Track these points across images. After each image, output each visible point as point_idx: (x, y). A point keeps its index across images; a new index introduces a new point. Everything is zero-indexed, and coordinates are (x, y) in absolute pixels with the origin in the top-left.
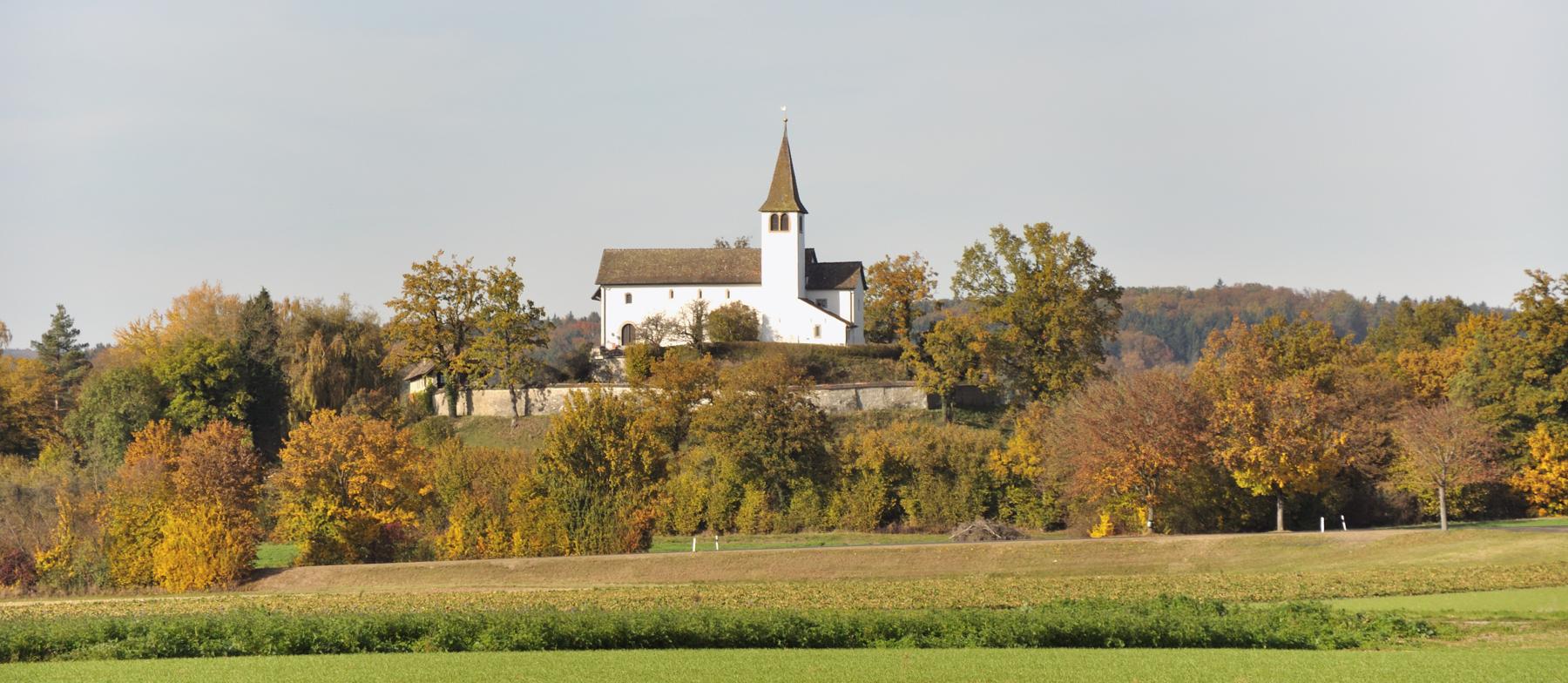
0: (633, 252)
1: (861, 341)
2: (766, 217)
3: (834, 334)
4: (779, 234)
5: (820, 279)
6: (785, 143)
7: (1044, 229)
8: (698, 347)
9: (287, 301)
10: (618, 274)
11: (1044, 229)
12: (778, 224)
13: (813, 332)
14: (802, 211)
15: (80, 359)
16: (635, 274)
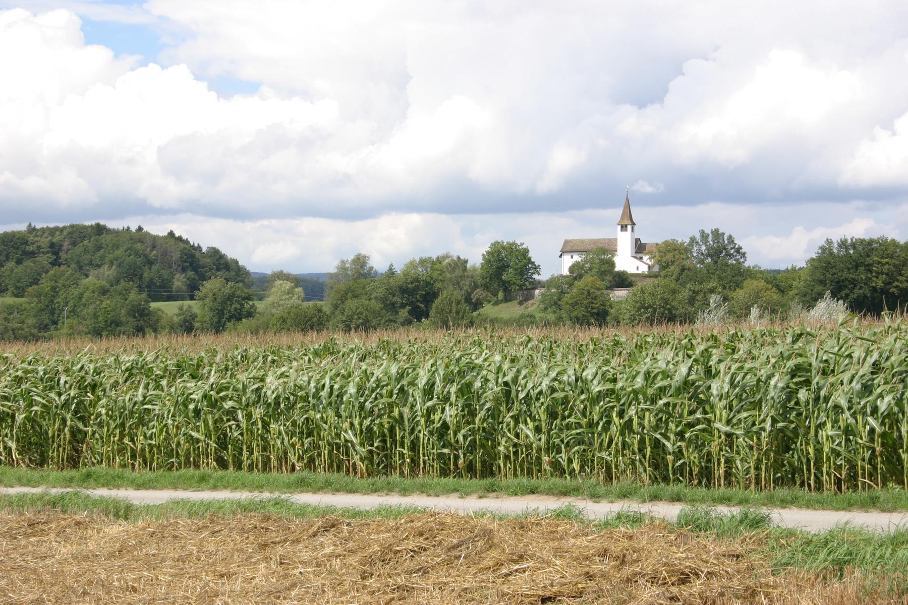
2: (619, 227)
3: (644, 269)
4: (624, 233)
5: (640, 248)
6: (627, 200)
7: (717, 230)
8: (679, 523)
9: (741, 248)
10: (568, 248)
11: (717, 230)
12: (624, 228)
14: (633, 224)
15: (393, 273)
16: (574, 248)
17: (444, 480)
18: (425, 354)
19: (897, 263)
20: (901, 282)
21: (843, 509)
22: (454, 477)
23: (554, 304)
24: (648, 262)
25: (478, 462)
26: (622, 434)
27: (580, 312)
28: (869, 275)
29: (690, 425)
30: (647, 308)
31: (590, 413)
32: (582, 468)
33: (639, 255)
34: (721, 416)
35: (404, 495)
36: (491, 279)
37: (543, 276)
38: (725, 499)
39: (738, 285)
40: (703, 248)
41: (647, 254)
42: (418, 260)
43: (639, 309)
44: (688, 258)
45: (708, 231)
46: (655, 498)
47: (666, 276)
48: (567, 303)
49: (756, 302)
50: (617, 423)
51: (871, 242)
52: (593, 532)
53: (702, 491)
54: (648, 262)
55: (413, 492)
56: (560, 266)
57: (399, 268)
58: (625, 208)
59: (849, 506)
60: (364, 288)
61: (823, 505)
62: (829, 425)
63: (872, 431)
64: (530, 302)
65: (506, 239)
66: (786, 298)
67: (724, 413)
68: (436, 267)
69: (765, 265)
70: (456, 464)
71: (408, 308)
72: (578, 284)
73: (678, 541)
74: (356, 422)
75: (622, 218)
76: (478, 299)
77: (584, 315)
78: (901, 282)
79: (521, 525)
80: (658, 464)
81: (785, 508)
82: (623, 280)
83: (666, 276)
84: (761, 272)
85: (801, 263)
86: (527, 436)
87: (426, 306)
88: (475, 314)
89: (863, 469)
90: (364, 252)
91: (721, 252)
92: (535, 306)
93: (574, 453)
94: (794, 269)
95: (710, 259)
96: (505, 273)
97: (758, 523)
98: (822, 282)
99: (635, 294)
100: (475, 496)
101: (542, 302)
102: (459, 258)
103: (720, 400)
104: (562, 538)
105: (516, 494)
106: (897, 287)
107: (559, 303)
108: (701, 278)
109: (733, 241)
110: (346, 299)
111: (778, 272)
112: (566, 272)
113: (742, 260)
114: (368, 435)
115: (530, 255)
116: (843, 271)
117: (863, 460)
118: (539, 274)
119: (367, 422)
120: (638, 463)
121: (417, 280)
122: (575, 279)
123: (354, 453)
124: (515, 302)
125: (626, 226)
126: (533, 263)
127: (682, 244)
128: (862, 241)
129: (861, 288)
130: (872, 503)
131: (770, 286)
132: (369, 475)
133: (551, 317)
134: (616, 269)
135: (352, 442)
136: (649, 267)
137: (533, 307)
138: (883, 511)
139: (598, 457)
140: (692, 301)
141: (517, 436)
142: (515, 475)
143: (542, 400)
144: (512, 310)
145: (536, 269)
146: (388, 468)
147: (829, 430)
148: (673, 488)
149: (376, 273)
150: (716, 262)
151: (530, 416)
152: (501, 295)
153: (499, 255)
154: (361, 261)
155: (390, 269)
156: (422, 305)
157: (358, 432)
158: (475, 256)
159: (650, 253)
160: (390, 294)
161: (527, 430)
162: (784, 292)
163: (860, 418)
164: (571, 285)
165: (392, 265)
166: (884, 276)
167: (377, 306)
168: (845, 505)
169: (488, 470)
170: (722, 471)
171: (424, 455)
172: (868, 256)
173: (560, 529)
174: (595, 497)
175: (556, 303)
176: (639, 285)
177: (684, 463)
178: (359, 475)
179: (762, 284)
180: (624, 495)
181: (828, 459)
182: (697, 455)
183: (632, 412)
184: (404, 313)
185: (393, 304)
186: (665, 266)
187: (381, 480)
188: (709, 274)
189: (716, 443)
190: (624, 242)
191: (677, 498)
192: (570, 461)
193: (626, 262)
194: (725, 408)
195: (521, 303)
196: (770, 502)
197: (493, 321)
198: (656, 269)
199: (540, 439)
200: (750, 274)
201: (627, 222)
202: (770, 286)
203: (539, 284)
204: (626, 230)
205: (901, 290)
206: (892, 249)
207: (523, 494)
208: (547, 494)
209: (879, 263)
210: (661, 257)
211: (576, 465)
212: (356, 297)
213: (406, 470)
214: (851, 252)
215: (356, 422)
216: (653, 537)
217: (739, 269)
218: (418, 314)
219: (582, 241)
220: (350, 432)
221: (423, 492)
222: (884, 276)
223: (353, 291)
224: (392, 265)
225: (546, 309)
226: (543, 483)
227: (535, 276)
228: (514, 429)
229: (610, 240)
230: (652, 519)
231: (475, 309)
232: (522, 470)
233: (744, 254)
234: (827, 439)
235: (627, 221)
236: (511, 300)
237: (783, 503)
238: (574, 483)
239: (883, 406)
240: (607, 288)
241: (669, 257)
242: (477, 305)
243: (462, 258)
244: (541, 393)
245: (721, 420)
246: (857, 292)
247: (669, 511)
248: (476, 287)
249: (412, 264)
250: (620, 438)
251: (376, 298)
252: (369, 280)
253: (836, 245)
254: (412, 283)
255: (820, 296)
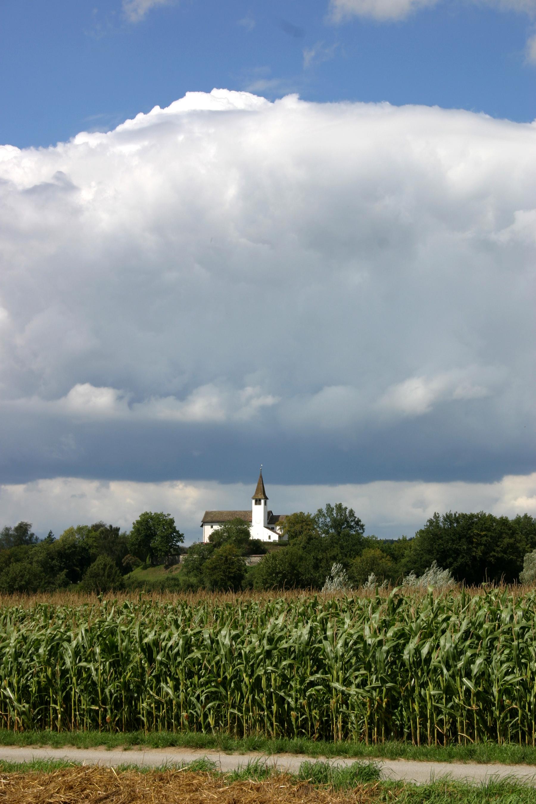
0: (215, 512)
1: (286, 538)
2: (254, 501)
3: (275, 537)
4: (258, 506)
5: (271, 521)
6: (261, 477)
7: (340, 505)
10: (209, 519)
11: (340, 505)
12: (258, 502)
13: (268, 538)
14: (266, 498)
15: (52, 540)
16: (214, 519)
17: (94, 733)
18: (76, 618)
19: (493, 535)
20: (498, 552)
21: (445, 761)
22: (102, 731)
23: (196, 568)
24: (279, 532)
25: (125, 717)
26: (252, 691)
27: (218, 576)
28: (470, 546)
29: (312, 684)
30: (277, 574)
31: (224, 673)
32: (217, 724)
33: (271, 526)
34: (338, 676)
35: (57, 748)
36: (139, 546)
37: (187, 544)
38: (343, 752)
39: (358, 553)
40: (328, 520)
41: (278, 525)
42: (75, 528)
43: (271, 574)
44: (314, 529)
45: (333, 505)
46: (281, 750)
47: (295, 544)
48: (207, 568)
49: (372, 570)
50: (247, 683)
51: (472, 516)
52: (225, 785)
53: (322, 745)
54: (279, 532)
55: (65, 745)
56: (202, 533)
57: (58, 536)
58: (258, 484)
59: (450, 758)
60: (26, 553)
61: (427, 757)
62: (431, 686)
63: (468, 690)
64: (175, 567)
65: (153, 510)
66: (399, 564)
67: (340, 673)
68: (91, 535)
69: (381, 537)
70: (104, 718)
71: (65, 571)
72: (219, 551)
73: (300, 792)
74: (15, 681)
75: (257, 493)
76: (128, 563)
77: (222, 579)
78: (498, 552)
79: (162, 776)
80: (283, 718)
81: (394, 759)
82: (258, 547)
83: (295, 544)
84: (378, 542)
85: (411, 534)
86: (167, 694)
87: (81, 570)
88: (126, 577)
89: (462, 723)
90: (26, 521)
91: (343, 524)
92: (179, 570)
93: (209, 709)
94: (405, 540)
95: (333, 531)
96: (152, 541)
97: (371, 774)
98: (430, 552)
99: (267, 560)
100: (120, 748)
101: (186, 566)
102: (111, 526)
103: (336, 662)
104: (197, 790)
105: (157, 747)
106: (494, 556)
107: (201, 567)
108: (323, 551)
109: (353, 515)
110: (10, 563)
111: (392, 542)
112: (206, 540)
113: (361, 531)
114: (24, 693)
115: (175, 524)
116: (448, 543)
117: (462, 716)
118: (183, 542)
119: (23, 681)
120: (266, 719)
121: (74, 546)
122: (215, 546)
123: (11, 709)
124: (162, 567)
125: (260, 500)
126: (177, 532)
127: (309, 516)
128: (464, 516)
129: (463, 557)
130: (469, 756)
131: (385, 554)
132: (25, 729)
133: (193, 580)
134: (251, 538)
135: (10, 698)
136: (280, 537)
137: (177, 571)
138: (480, 762)
139: (231, 713)
140: (316, 567)
141: (158, 692)
142: (157, 730)
143: (179, 659)
144: (159, 574)
145: (180, 537)
146: (43, 723)
147: (432, 691)
148: (296, 741)
149: (37, 539)
150: (339, 533)
151: (170, 676)
152: (148, 561)
153: (147, 524)
154: (23, 528)
155: (50, 536)
156: (78, 569)
157: (16, 689)
158: (126, 524)
159: (281, 524)
160: (50, 558)
161: (168, 688)
162: (397, 561)
163: (458, 679)
164: (211, 552)
165: (51, 532)
166: (483, 547)
167: (36, 568)
168: (446, 757)
169: (133, 724)
170: (339, 725)
171: (75, 710)
172: (470, 529)
173: (195, 781)
174: (228, 749)
175: (197, 568)
176: (272, 552)
177: (306, 718)
178: (16, 728)
179: (378, 552)
180: (255, 747)
181: (432, 714)
182: (318, 712)
183: (260, 672)
184: (62, 575)
185: (52, 568)
186: (293, 535)
187: (36, 735)
188: (333, 542)
189: (334, 700)
190: (258, 513)
191: (300, 751)
192: (206, 716)
193: (259, 532)
194: (342, 669)
195: (167, 567)
196: (382, 754)
197: (140, 585)
198: (286, 538)
199: (178, 697)
200: (369, 543)
201: (261, 496)
202: (385, 554)
203: (183, 551)
204: (260, 504)
205: (497, 559)
206: (490, 523)
207: (164, 746)
208: (185, 747)
209: (478, 535)
210: (291, 527)
211: (211, 720)
212: (17, 561)
213: (58, 724)
214: (455, 525)
215: (15, 681)
216: (278, 788)
217: (358, 539)
218: (74, 577)
219: (221, 513)
220: (8, 689)
221: (73, 745)
222: (483, 547)
223: (16, 555)
224: (51, 532)
225: (189, 572)
226: (183, 736)
227: (180, 544)
228: (156, 687)
229: (246, 512)
230: (277, 774)
231: (126, 573)
232: (163, 725)
233: (362, 526)
234: (430, 698)
235: (260, 496)
236: (157, 565)
237: (394, 755)
238: (209, 737)
239: (475, 669)
240: (243, 555)
241: (298, 527)
242: (127, 569)
243: (114, 526)
244: (178, 654)
245: (338, 680)
246: (460, 560)
247: (291, 763)
248: (126, 552)
249: (71, 532)
250: (251, 697)
251: (37, 562)
252: (30, 546)
253: (442, 519)
254: (69, 548)
255: (428, 565)
